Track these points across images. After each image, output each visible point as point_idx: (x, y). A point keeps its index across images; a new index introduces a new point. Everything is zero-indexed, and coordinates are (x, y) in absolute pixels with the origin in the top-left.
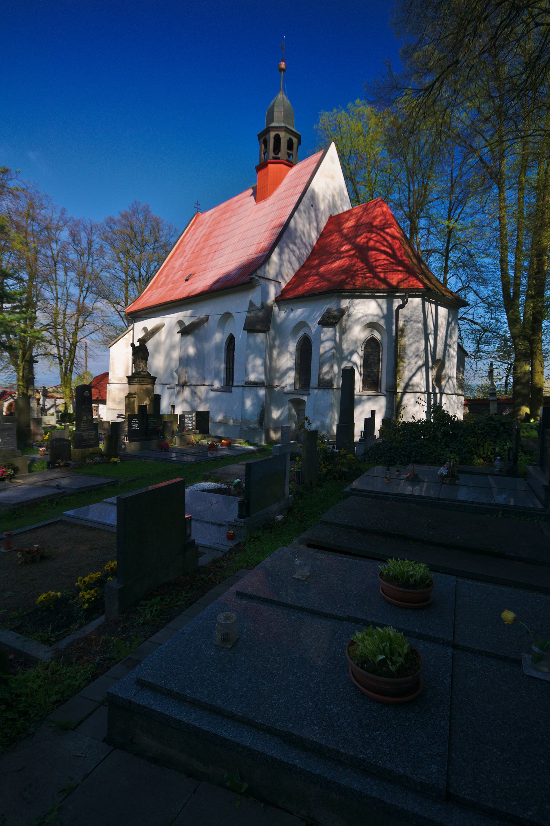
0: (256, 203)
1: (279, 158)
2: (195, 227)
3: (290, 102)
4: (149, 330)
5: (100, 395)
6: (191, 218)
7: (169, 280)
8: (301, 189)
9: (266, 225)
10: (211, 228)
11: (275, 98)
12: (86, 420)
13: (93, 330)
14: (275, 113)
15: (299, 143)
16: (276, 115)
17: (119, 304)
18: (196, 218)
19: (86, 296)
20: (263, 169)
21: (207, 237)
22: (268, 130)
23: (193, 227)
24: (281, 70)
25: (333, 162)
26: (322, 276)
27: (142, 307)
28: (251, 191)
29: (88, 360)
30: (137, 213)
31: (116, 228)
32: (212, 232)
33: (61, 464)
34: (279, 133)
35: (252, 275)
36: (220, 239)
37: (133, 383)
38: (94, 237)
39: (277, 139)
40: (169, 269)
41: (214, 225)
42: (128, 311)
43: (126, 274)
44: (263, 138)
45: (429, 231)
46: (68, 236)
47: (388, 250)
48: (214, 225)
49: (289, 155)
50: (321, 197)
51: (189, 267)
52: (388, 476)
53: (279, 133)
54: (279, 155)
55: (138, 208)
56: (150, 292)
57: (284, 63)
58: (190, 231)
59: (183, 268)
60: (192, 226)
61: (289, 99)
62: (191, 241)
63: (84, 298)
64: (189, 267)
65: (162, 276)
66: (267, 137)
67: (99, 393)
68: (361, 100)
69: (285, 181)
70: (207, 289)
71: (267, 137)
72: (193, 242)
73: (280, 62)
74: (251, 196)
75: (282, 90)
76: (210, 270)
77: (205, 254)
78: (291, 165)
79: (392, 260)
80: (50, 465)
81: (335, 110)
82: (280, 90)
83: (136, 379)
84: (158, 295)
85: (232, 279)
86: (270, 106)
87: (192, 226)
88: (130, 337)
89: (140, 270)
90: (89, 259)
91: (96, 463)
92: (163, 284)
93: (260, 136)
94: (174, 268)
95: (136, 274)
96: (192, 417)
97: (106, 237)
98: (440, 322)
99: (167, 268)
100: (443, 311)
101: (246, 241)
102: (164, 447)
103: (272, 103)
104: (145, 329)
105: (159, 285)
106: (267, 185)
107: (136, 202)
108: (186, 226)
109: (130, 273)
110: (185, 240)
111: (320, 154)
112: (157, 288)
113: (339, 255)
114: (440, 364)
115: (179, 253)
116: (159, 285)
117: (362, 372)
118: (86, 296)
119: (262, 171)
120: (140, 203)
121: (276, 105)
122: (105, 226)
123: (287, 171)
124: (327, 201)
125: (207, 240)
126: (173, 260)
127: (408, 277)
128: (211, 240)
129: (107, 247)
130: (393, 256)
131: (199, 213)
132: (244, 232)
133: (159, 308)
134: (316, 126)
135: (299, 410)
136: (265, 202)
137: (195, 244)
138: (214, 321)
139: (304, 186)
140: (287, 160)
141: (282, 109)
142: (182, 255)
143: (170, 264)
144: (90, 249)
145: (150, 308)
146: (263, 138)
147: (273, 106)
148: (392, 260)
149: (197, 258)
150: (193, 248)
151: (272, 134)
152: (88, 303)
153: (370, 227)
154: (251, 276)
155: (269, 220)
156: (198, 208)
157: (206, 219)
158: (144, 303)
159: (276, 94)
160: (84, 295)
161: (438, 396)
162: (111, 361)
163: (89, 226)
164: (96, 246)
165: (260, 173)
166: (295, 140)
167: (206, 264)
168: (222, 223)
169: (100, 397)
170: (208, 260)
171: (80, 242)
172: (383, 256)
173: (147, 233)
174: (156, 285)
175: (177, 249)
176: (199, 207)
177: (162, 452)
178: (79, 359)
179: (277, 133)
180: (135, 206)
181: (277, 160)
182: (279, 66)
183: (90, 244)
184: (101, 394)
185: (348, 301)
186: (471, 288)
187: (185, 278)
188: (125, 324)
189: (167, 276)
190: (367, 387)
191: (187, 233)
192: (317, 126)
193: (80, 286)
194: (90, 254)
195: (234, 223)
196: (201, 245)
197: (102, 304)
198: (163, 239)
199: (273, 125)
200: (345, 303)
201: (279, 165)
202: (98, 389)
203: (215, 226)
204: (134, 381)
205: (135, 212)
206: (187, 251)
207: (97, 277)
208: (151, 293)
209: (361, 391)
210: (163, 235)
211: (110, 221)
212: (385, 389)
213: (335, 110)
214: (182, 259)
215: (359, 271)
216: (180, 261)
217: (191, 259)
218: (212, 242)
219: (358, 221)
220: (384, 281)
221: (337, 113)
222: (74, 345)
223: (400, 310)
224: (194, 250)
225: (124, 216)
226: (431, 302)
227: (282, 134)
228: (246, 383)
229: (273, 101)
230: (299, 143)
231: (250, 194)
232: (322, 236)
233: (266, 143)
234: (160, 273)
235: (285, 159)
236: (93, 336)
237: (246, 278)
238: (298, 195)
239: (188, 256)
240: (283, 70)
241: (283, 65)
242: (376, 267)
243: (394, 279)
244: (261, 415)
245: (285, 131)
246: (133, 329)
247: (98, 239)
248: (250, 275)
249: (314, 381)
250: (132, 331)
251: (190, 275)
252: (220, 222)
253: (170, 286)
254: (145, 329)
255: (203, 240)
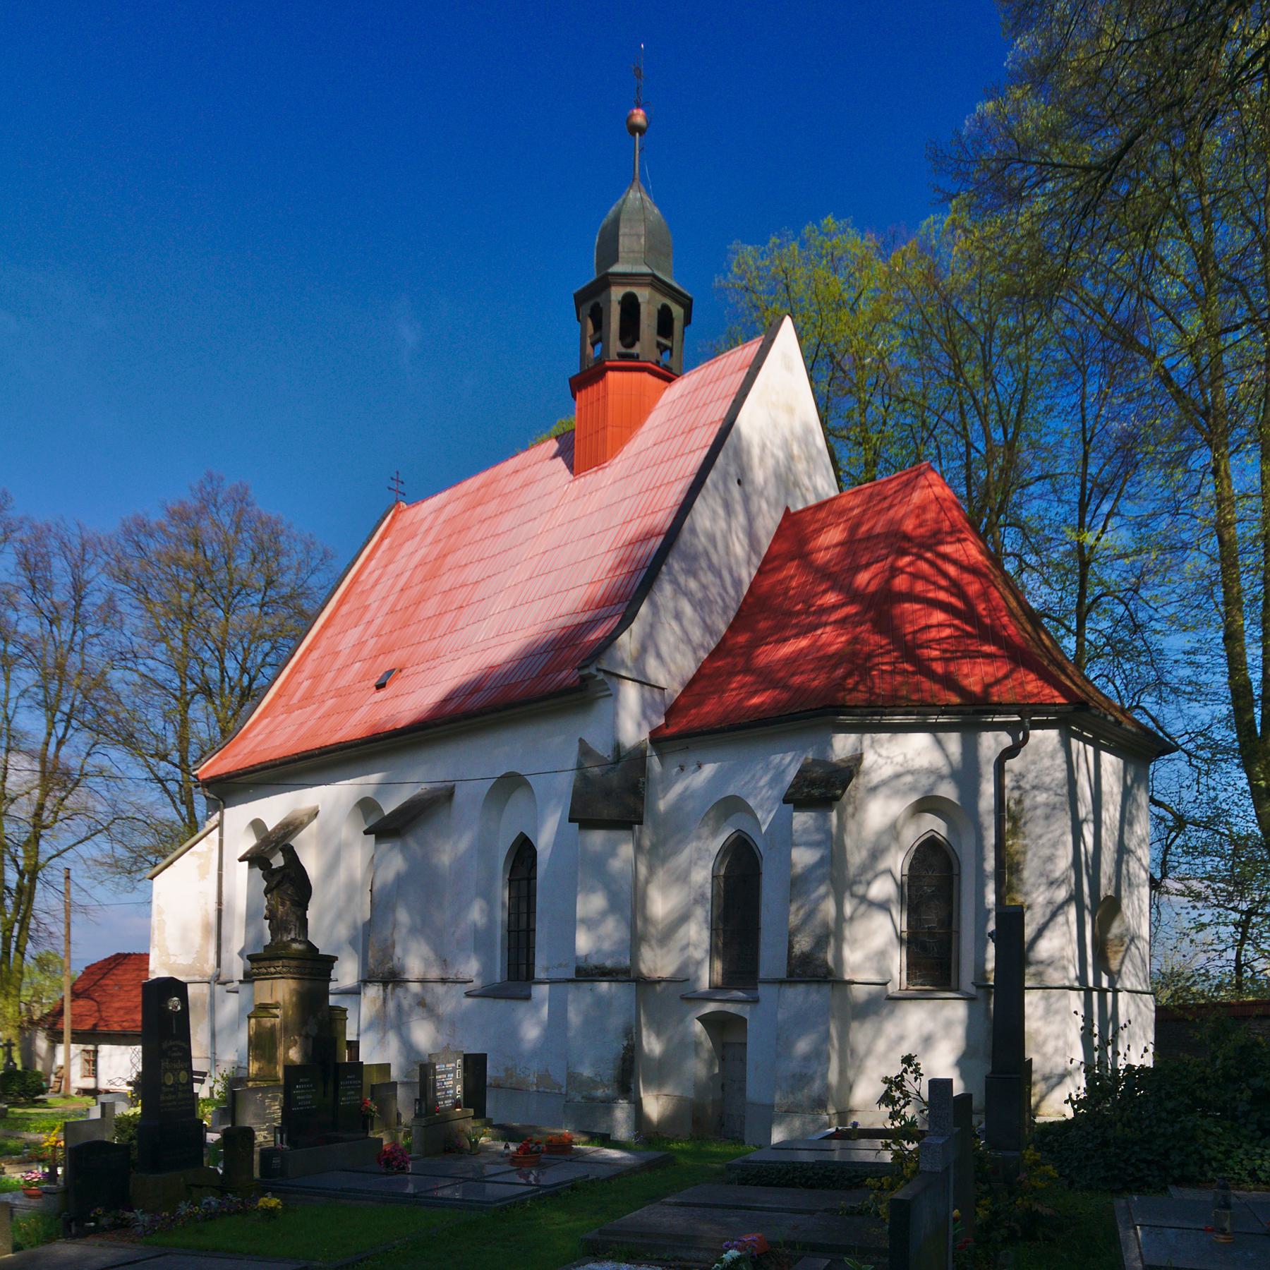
0: (572, 477)
1: (635, 357)
2: (393, 541)
3: (660, 209)
4: (270, 828)
5: (101, 1018)
6: (378, 518)
7: (321, 689)
8: (706, 437)
9: (611, 535)
10: (441, 545)
11: (620, 201)
12: (172, 1086)
13: (84, 832)
14: (621, 239)
15: (687, 320)
16: (624, 243)
17: (164, 758)
18: (393, 517)
19: (64, 736)
20: (592, 385)
21: (433, 569)
22: (604, 283)
23: (387, 542)
24: (634, 129)
25: (789, 368)
26: (767, 678)
27: (246, 764)
28: (553, 446)
29: (73, 917)
30: (215, 506)
31: (153, 547)
32: (445, 556)
33: (104, 1221)
34: (635, 290)
35: (587, 666)
36: (473, 573)
37: (267, 973)
38: (90, 573)
39: (630, 306)
40: (322, 658)
41: (450, 536)
42: (205, 776)
43: (184, 677)
44: (591, 303)
45: (1021, 560)
46: (12, 568)
47: (953, 600)
48: (450, 536)
49: (662, 348)
50: (756, 452)
51: (385, 651)
52: (1227, 1225)
53: (635, 290)
54: (636, 350)
55: (217, 494)
56: (265, 722)
57: (641, 112)
58: (379, 554)
59: (366, 652)
60: (382, 539)
61: (657, 203)
62: (384, 579)
63: (60, 743)
64: (385, 651)
65: (299, 677)
66: (600, 299)
67: (99, 1011)
68: (838, 217)
69: (656, 418)
70: (423, 715)
71: (600, 299)
72: (390, 582)
73: (632, 108)
74: (555, 457)
75: (637, 181)
76: (449, 657)
77: (430, 613)
78: (668, 376)
79: (969, 629)
80: (73, 1224)
81: (774, 240)
82: (634, 180)
83: (280, 963)
84: (293, 728)
85: (523, 681)
86: (605, 221)
87: (382, 539)
88: (211, 850)
89: (222, 661)
90: (74, 632)
91: (210, 1216)
92: (308, 698)
93: (580, 298)
94: (337, 653)
95: (214, 674)
96: (454, 1071)
97: (127, 573)
98: (1105, 786)
99: (315, 655)
100: (1110, 762)
101: (553, 576)
102: (395, 1159)
103: (611, 213)
104: (257, 825)
105: (295, 700)
106: (604, 428)
107: (210, 476)
108: (364, 540)
109: (195, 669)
110: (363, 578)
111: (753, 348)
112: (289, 710)
113: (815, 619)
114: (1108, 909)
115: (350, 613)
116: (295, 700)
117: (905, 935)
118: (64, 736)
119: (589, 389)
120: (222, 479)
121: (623, 217)
122: (123, 542)
123: (660, 393)
124: (770, 462)
125: (433, 575)
126: (330, 632)
127: (1012, 671)
128: (445, 578)
129: (127, 605)
130: (968, 615)
131: (402, 504)
132: (544, 553)
133: (300, 765)
134: (719, 281)
135: (724, 1045)
136: (600, 473)
137: (398, 588)
138: (471, 793)
139: (716, 429)
140: (658, 363)
141: (641, 229)
142: (361, 618)
143: (324, 643)
144: (78, 605)
145: (274, 766)
146: (591, 303)
147: (616, 222)
148: (969, 629)
149: (406, 625)
150: (392, 598)
151: (617, 293)
152: (71, 757)
153: (898, 541)
154: (586, 672)
155: (618, 519)
156: (398, 491)
157: (423, 520)
158: (253, 752)
159: (621, 190)
160: (60, 735)
161: (1109, 995)
162: (155, 919)
163: (76, 542)
164: (94, 599)
165: (582, 395)
166: (677, 311)
167: (435, 643)
168: (475, 529)
169: (102, 1023)
170: (441, 631)
171: (49, 586)
172: (939, 616)
173: (242, 563)
174: (283, 701)
175: (341, 603)
176: (401, 488)
177: (387, 1174)
178: (46, 919)
179: (628, 289)
180: (209, 489)
181: (630, 363)
182: (629, 118)
183: (78, 590)
184: (104, 1014)
185: (853, 737)
186: (1142, 708)
187: (375, 681)
188: (179, 813)
189: (317, 677)
190: (920, 977)
191: (369, 558)
192: (723, 282)
193: (50, 708)
194: (78, 621)
195: (511, 530)
196: (415, 592)
197: (115, 757)
198: (288, 578)
199: (617, 268)
200: (843, 745)
201: (635, 376)
202: (92, 999)
203: (452, 540)
204: (272, 970)
205: (208, 503)
206: (374, 606)
207: (101, 682)
208: (270, 723)
209: (904, 986)
210: (289, 568)
211: (137, 530)
212: (972, 980)
213: (774, 240)
214: (361, 628)
215: (879, 655)
216: (353, 636)
217: (387, 629)
218: (446, 581)
219: (853, 529)
220: (949, 682)
221: (780, 246)
222: (31, 873)
223: (1012, 764)
224: (394, 605)
225: (180, 515)
226: (1086, 741)
227: (643, 294)
228: (579, 971)
229: (613, 208)
230: (687, 320)
231: (551, 455)
232: (768, 565)
233: (598, 317)
234: (294, 667)
235: (654, 361)
236: (85, 850)
237: (567, 676)
238: (698, 453)
239: (378, 622)
240: (641, 130)
241: (639, 117)
242: (927, 644)
243: (975, 675)
244: (624, 1060)
245: (651, 285)
246: (220, 824)
247: (103, 577)
248: (580, 669)
249: (771, 961)
250: (217, 831)
251: (390, 673)
252: (469, 528)
253: (330, 703)
254: (257, 825)
255: (419, 575)
